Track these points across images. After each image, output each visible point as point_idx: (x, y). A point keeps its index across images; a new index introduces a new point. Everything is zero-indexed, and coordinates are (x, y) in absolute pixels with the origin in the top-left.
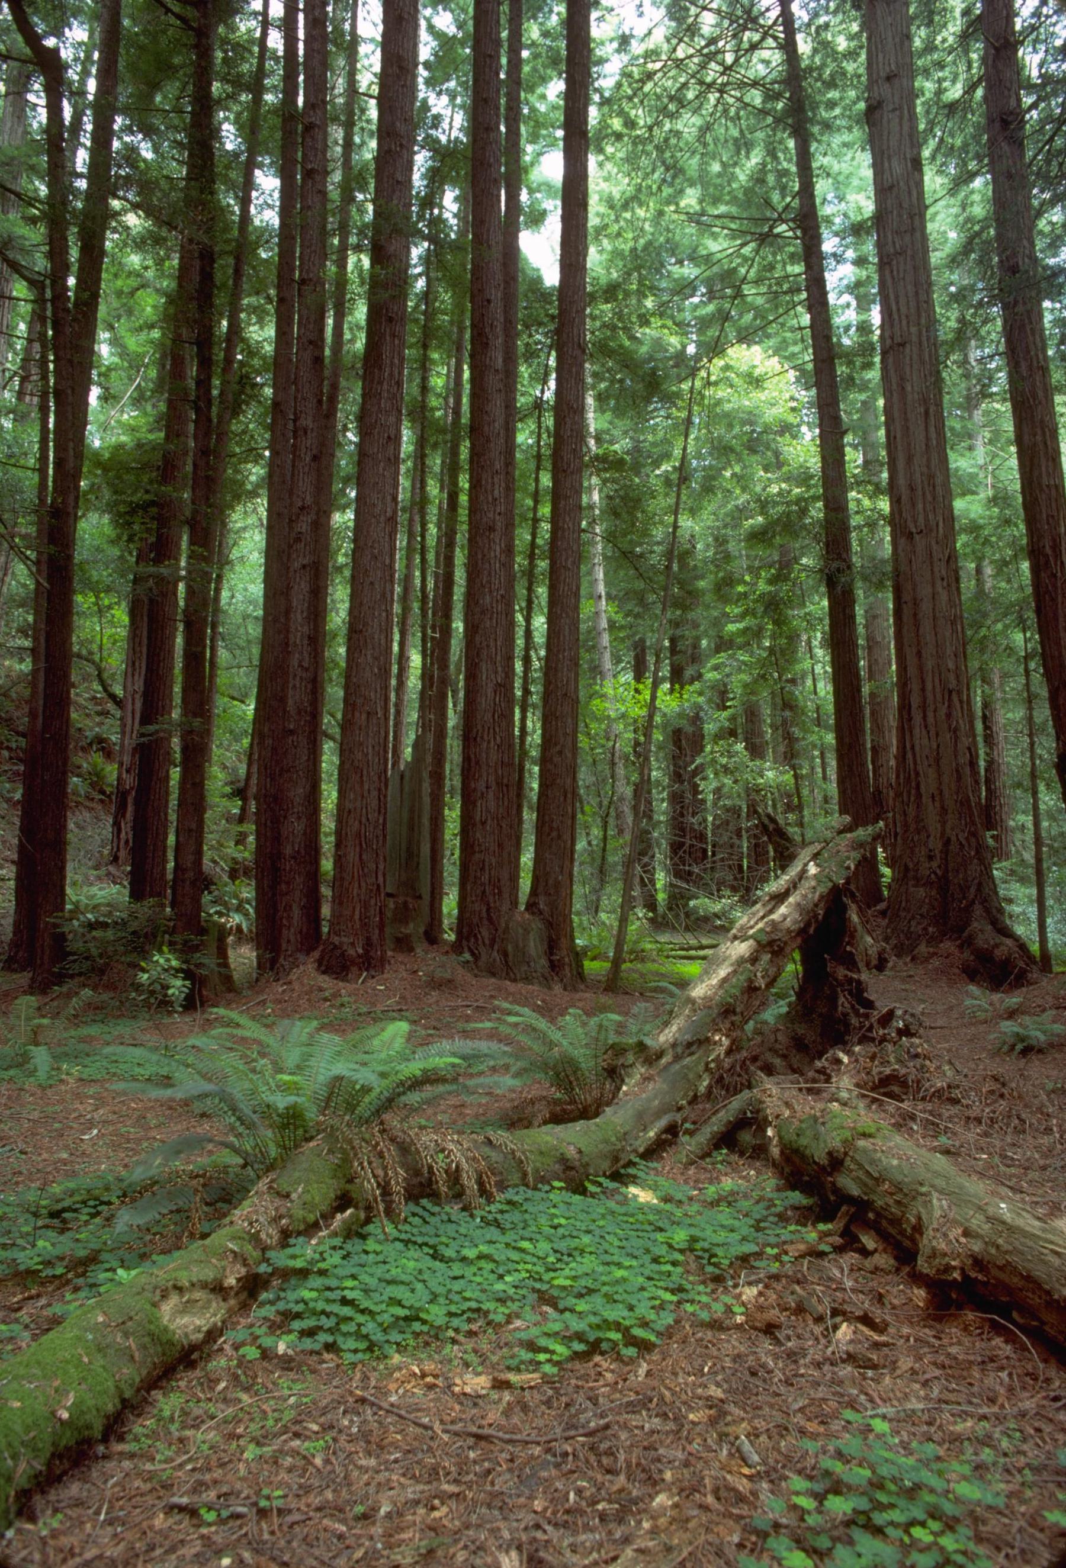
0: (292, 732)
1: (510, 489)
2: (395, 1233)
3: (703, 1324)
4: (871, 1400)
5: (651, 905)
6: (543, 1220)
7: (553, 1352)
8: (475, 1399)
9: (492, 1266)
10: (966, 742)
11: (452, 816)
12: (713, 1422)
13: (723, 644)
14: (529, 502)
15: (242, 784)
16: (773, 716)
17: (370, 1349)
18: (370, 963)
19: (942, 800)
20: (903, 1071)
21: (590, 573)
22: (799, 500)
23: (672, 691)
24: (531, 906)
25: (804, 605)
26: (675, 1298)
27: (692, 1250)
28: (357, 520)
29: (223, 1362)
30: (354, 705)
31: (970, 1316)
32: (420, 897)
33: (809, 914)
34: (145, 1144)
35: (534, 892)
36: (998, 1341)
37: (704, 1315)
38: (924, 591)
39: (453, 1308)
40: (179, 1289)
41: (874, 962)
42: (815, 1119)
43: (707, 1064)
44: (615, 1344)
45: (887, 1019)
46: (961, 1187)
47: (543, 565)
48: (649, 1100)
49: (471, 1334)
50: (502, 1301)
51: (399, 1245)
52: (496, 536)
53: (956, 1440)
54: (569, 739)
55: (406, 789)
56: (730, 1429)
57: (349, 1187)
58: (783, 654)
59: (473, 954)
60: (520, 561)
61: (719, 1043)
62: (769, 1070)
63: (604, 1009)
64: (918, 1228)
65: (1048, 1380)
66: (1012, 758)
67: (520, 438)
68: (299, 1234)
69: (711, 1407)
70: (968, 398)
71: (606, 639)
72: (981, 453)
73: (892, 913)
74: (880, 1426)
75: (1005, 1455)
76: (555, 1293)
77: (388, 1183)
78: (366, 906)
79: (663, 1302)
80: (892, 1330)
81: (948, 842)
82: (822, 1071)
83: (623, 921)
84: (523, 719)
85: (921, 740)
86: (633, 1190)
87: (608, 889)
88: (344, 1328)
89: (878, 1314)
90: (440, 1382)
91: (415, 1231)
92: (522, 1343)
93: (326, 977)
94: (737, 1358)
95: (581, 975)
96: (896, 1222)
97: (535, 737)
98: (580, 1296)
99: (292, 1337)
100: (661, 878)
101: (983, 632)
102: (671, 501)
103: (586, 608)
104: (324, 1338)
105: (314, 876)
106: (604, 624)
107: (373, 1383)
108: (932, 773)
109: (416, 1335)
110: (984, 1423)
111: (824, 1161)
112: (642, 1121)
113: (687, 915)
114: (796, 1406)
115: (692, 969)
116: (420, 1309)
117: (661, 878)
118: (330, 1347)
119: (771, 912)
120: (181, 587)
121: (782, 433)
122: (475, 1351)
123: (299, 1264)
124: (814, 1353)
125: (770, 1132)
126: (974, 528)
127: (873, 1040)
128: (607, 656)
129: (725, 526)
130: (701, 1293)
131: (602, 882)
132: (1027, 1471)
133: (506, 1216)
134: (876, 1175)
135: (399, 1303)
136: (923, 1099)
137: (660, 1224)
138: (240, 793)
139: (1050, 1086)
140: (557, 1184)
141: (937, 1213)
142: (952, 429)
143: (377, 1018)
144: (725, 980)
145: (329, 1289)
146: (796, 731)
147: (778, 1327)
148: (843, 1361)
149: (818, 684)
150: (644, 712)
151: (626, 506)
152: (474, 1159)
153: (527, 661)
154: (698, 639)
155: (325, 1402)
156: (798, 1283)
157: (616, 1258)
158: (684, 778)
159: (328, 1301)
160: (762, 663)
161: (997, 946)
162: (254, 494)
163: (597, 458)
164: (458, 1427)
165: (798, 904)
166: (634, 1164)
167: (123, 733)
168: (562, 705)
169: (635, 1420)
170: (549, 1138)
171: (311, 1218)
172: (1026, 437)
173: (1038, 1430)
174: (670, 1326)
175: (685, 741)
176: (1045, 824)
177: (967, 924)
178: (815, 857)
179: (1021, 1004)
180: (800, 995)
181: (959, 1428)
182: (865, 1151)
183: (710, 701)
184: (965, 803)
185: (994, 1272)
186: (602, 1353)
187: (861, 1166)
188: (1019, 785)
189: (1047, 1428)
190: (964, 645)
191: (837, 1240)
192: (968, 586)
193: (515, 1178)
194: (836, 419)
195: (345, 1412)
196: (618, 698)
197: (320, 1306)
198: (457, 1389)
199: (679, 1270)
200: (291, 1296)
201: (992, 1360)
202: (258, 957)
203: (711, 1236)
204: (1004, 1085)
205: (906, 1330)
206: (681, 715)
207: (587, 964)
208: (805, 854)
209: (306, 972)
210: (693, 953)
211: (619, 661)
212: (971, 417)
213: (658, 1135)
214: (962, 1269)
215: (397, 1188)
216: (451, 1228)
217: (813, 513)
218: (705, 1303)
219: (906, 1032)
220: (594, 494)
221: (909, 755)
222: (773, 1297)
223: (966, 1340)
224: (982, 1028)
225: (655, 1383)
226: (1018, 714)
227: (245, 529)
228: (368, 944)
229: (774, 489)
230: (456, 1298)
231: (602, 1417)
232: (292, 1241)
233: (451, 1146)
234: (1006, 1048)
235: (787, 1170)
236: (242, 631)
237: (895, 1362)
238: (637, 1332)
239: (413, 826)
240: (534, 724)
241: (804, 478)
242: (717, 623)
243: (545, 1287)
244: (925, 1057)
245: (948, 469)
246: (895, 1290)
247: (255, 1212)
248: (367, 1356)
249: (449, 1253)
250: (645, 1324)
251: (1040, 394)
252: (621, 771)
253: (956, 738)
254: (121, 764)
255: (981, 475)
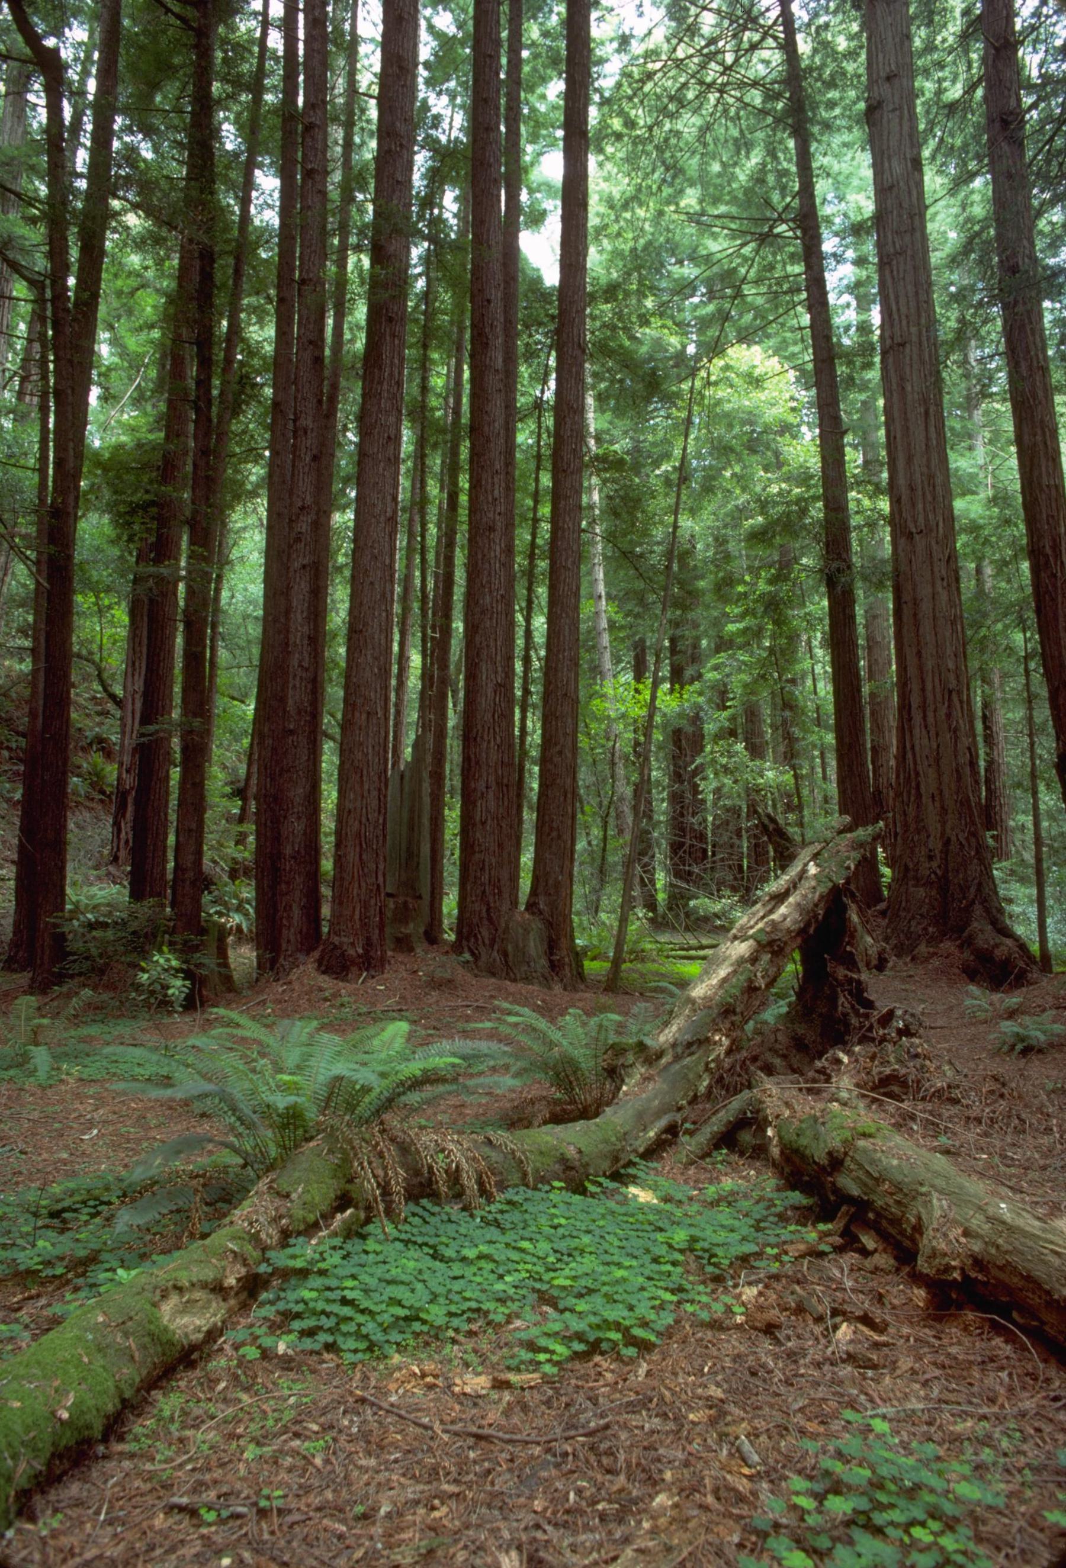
0: (292, 732)
1: (510, 489)
2: (395, 1233)
3: (703, 1324)
4: (871, 1400)
5: (651, 905)
6: (543, 1220)
7: (553, 1352)
8: (475, 1399)
9: (492, 1266)
10: (966, 742)
11: (452, 816)
12: (713, 1422)
13: (723, 644)
14: (529, 502)
15: (242, 784)
16: (773, 716)
17: (370, 1349)
18: (370, 963)
19: (942, 800)
20: (903, 1071)
21: (590, 573)
22: (799, 500)
23: (672, 691)
24: (531, 906)
25: (804, 605)
26: (675, 1298)
27: (692, 1250)
28: (357, 520)
29: (223, 1362)
30: (354, 705)
31: (970, 1316)
32: (420, 897)
33: (809, 914)
34: (145, 1144)
35: (534, 892)
36: (998, 1341)
37: (704, 1315)
38: (924, 591)
39: (453, 1308)
40: (179, 1289)
41: (874, 962)
42: (815, 1119)
43: (707, 1064)
44: (615, 1344)
45: (887, 1019)
46: (961, 1187)
47: (543, 565)
48: (649, 1100)
49: (471, 1334)
50: (502, 1301)
51: (399, 1245)
52: (496, 536)
53: (956, 1440)
54: (569, 739)
55: (406, 789)
56: (730, 1429)
57: (349, 1187)
58: (783, 654)
59: (473, 954)
60: (520, 561)
61: (719, 1043)
62: (769, 1070)
63: (604, 1009)
64: (918, 1228)
65: (1048, 1380)
66: (1012, 758)
67: (520, 438)
68: (299, 1234)
69: (711, 1407)
70: (968, 398)
71: (606, 639)
72: (981, 453)
73: (892, 913)
74: (880, 1426)
75: (1005, 1455)
76: (555, 1293)
77: (388, 1183)
78: (366, 906)
79: (663, 1302)
80: (892, 1330)
81: (948, 842)
82: (822, 1071)
83: (623, 921)
84: (523, 719)
85: (921, 740)
86: (633, 1190)
87: (608, 889)
88: (344, 1328)
89: (878, 1314)
90: (440, 1382)
91: (415, 1231)
92: (522, 1343)
93: (326, 977)
94: (737, 1358)
95: (581, 975)
96: (896, 1222)
97: (535, 737)
98: (580, 1296)
99: (292, 1337)
100: (661, 878)
101: (983, 632)
102: (671, 501)
103: (586, 608)
104: (324, 1338)
105: (314, 876)
106: (604, 624)
107: (373, 1383)
108: (932, 773)
109: (416, 1335)
110: (984, 1423)
111: (824, 1161)
112: (642, 1121)
113: (687, 915)
114: (796, 1406)
115: (692, 969)
116: (420, 1309)
117: (661, 878)
118: (330, 1347)
119: (771, 912)
120: (181, 587)
121: (782, 433)
122: (475, 1351)
123: (299, 1264)
124: (814, 1353)
125: (770, 1132)
126: (974, 528)
127: (873, 1040)
128: (607, 656)
129: (725, 526)
130: (701, 1293)
131: (602, 882)
132: (1027, 1471)
133: (506, 1216)
134: (876, 1175)
135: (399, 1303)
136: (923, 1099)
137: (660, 1224)
138: (240, 793)
139: (1050, 1086)
140: (557, 1184)
141: (937, 1213)
142: (952, 429)
143: (377, 1018)
144: (725, 980)
145: (329, 1289)
146: (796, 731)
147: (778, 1327)
148: (843, 1361)
149: (818, 684)
150: (644, 712)
151: (626, 506)
152: (474, 1159)
153: (527, 661)
154: (698, 639)
155: (325, 1402)
156: (798, 1283)
157: (616, 1258)
158: (684, 778)
159: (328, 1301)
160: (762, 663)
161: (997, 946)
162: (254, 494)
163: (597, 458)
164: (458, 1427)
165: (798, 904)
166: (634, 1164)
167: (123, 733)
168: (562, 705)
169: (635, 1420)
170: (549, 1138)
171: (311, 1218)
172: (1026, 437)
173: (1038, 1430)
174: (670, 1326)
175: (685, 741)
176: (1045, 824)
177: (967, 924)
178: (815, 857)
179: (1021, 1004)
180: (800, 995)
181: (959, 1428)
182: (865, 1151)
183: (710, 701)
184: (965, 803)
185: (994, 1272)
186: (602, 1353)
187: (861, 1166)
188: (1019, 785)
189: (1047, 1428)
190: (964, 645)
191: (837, 1240)
192: (968, 586)
193: (515, 1178)
194: (836, 419)
195: (345, 1412)
196: (618, 698)
197: (320, 1306)
198: (457, 1389)
199: (679, 1270)
200: (291, 1296)
201: (992, 1360)
202: (258, 957)
203: (711, 1236)
204: (1004, 1085)
205: (906, 1330)
206: (681, 715)
207: (587, 964)
208: (805, 854)
209: (306, 972)
210: (693, 953)
211: (619, 661)
212: (971, 417)
213: (658, 1135)
214: (962, 1269)
215: (397, 1188)
216: (451, 1228)
217: (813, 513)
218: (705, 1303)
219: (906, 1032)
220: (594, 494)
221: (909, 755)
222: (773, 1297)
223: (966, 1340)
224: (982, 1028)
225: (655, 1383)
226: (1018, 714)
227: (245, 529)
228: (368, 944)
229: (774, 489)
230: (456, 1298)
231: (602, 1417)
232: (292, 1241)
233: (451, 1146)
234: (1006, 1048)
235: (787, 1170)
236: (242, 631)
237: (895, 1362)
238: (637, 1332)
239: (413, 826)
240: (534, 724)
241: (804, 478)
242: (717, 623)
243: (545, 1287)
244: (925, 1057)
245: (948, 469)
246: (895, 1290)
247: (255, 1212)
248: (367, 1356)
249: (449, 1253)
250: (645, 1324)
251: (1040, 394)
252: (621, 771)
253: (956, 738)
254: (121, 764)
255: (981, 475)
